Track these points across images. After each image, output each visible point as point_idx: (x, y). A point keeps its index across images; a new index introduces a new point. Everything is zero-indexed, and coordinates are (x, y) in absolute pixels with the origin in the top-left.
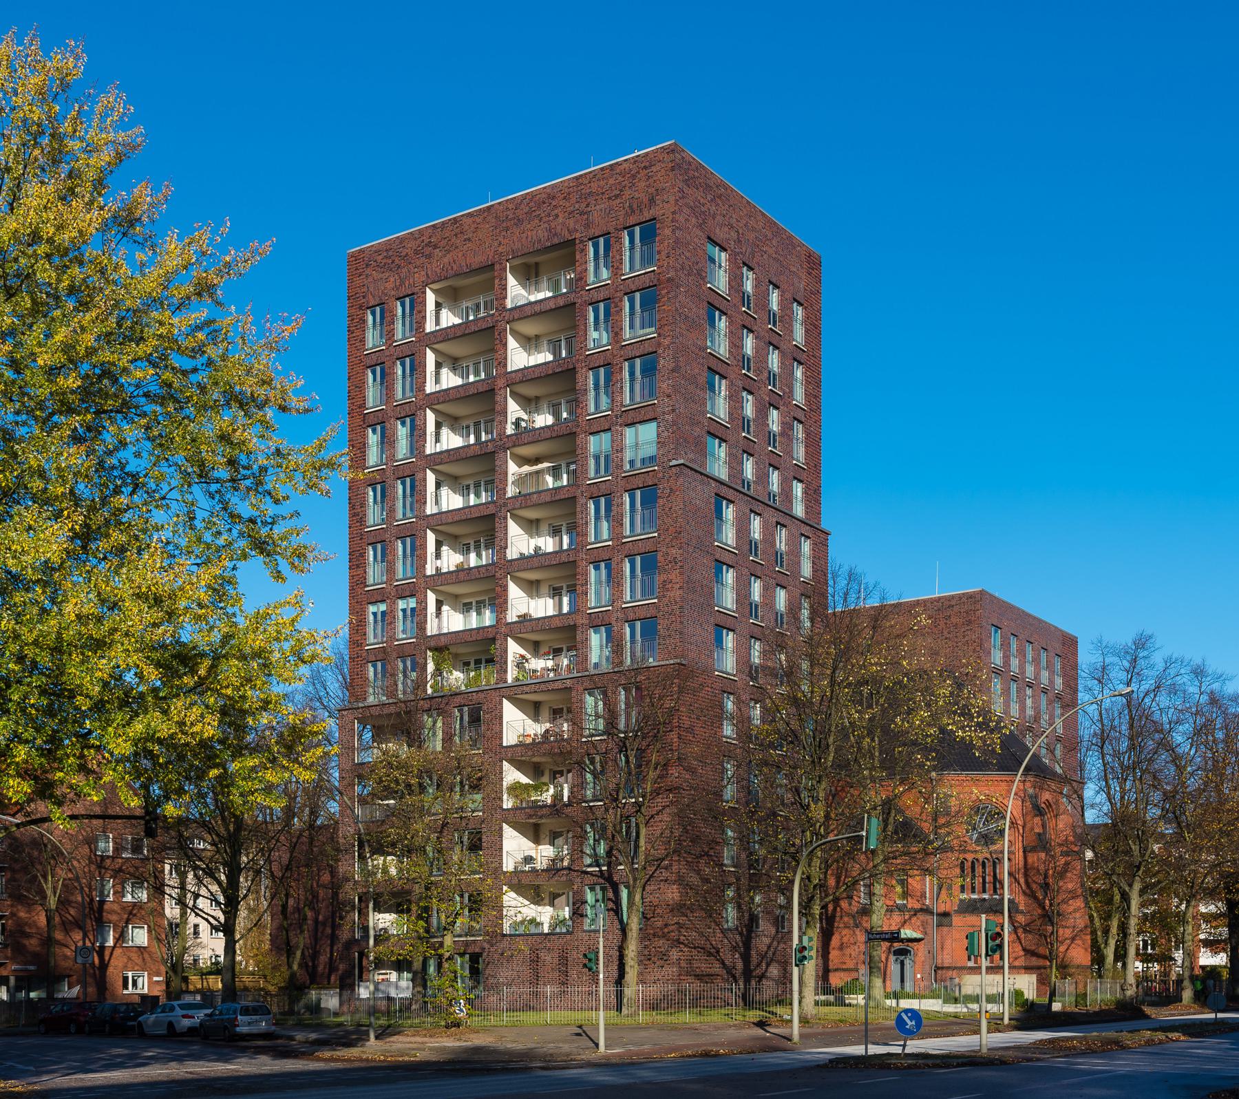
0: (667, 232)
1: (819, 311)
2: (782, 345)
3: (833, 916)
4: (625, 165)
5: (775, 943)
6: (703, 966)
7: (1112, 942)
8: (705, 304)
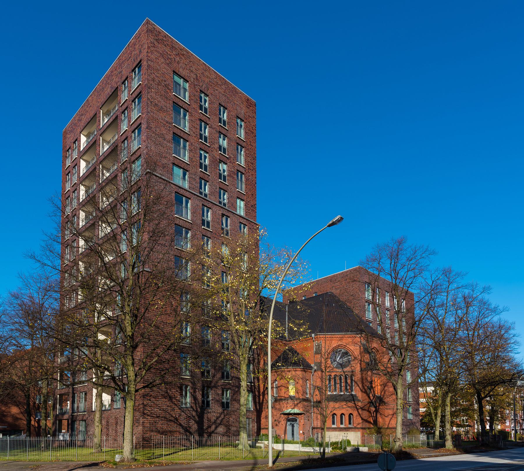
0: (145, 63)
1: (255, 126)
2: (228, 135)
3: (263, 403)
4: (132, 42)
5: (222, 416)
6: (161, 425)
7: (439, 419)
8: (171, 102)
